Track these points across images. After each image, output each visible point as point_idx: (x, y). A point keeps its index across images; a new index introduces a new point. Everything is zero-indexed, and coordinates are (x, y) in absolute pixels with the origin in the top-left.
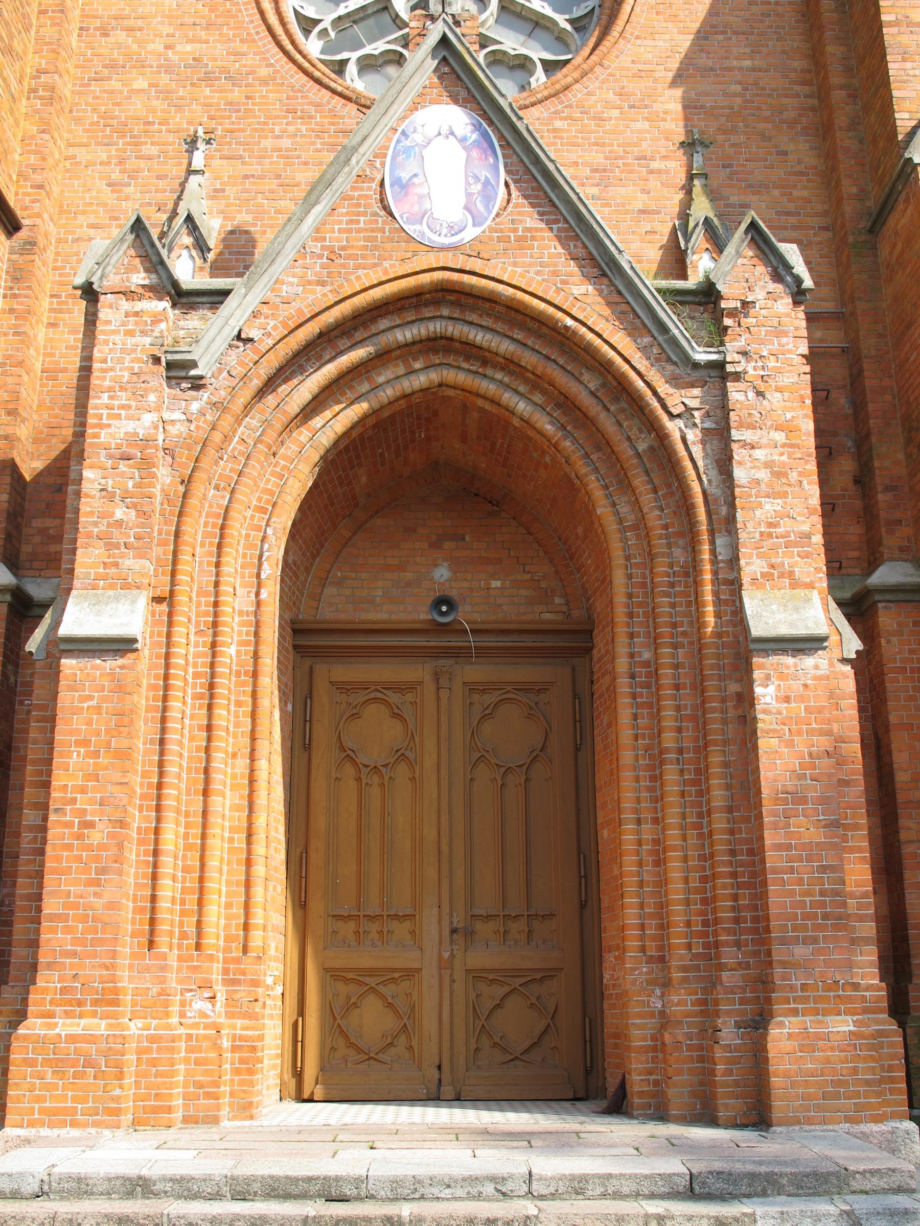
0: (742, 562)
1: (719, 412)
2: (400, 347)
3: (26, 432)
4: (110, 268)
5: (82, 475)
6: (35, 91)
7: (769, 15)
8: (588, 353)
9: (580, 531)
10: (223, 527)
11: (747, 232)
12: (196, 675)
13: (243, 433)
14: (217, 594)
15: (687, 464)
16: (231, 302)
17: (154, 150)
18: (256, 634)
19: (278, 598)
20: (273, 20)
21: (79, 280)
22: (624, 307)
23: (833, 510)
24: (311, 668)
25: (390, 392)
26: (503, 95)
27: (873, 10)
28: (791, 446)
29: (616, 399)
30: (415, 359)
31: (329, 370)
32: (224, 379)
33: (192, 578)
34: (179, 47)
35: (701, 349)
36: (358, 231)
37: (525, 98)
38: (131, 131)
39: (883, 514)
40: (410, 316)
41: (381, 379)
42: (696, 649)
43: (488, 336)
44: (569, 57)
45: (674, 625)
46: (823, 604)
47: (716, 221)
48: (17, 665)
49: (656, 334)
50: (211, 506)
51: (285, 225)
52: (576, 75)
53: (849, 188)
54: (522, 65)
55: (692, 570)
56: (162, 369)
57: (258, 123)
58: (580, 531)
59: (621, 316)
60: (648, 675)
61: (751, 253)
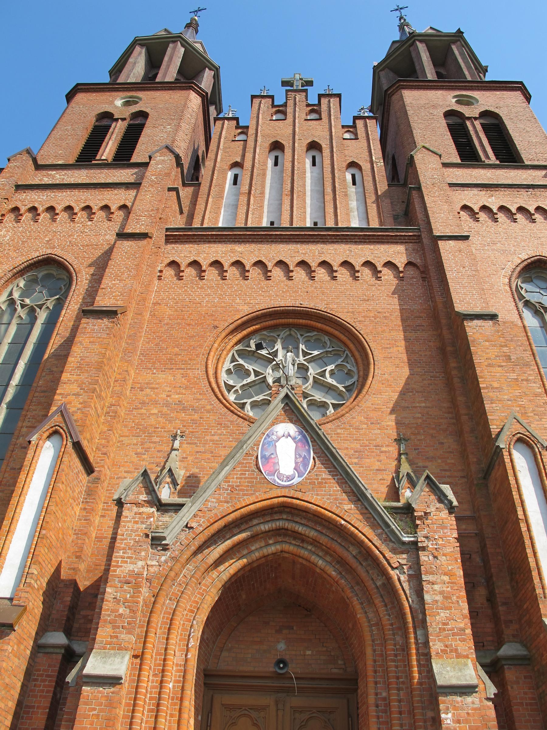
0: (431, 644)
1: (416, 566)
2: (263, 533)
3: (84, 567)
4: (130, 492)
5: (105, 590)
6: (109, 413)
7: (432, 385)
8: (352, 537)
9: (350, 625)
10: (172, 620)
11: (425, 480)
12: (151, 699)
13: (185, 573)
14: (166, 655)
15: (401, 592)
16: (184, 510)
17: (157, 439)
18: (184, 677)
19: (196, 658)
20: (214, 385)
21: (116, 497)
22: (368, 515)
23: (477, 615)
24: (212, 696)
25: (257, 554)
26: (312, 419)
27: (476, 383)
28: (452, 583)
29: (366, 560)
30: (269, 539)
31: (229, 543)
32: (178, 546)
33: (154, 646)
34: (173, 396)
35: (405, 535)
36: (245, 478)
37: (324, 420)
38: (148, 430)
39: (502, 618)
40: (268, 518)
41: (253, 548)
42: (410, 691)
43: (305, 528)
44: (344, 402)
45: (398, 678)
46: (474, 667)
47: (412, 474)
48: (62, 688)
49: (384, 528)
50: (167, 608)
51: (212, 475)
52: (347, 410)
53: (473, 459)
54: (323, 405)
55: (406, 648)
56: (149, 540)
57: (205, 429)
58: (350, 625)
59: (367, 519)
60: (386, 705)
61: (427, 490)
